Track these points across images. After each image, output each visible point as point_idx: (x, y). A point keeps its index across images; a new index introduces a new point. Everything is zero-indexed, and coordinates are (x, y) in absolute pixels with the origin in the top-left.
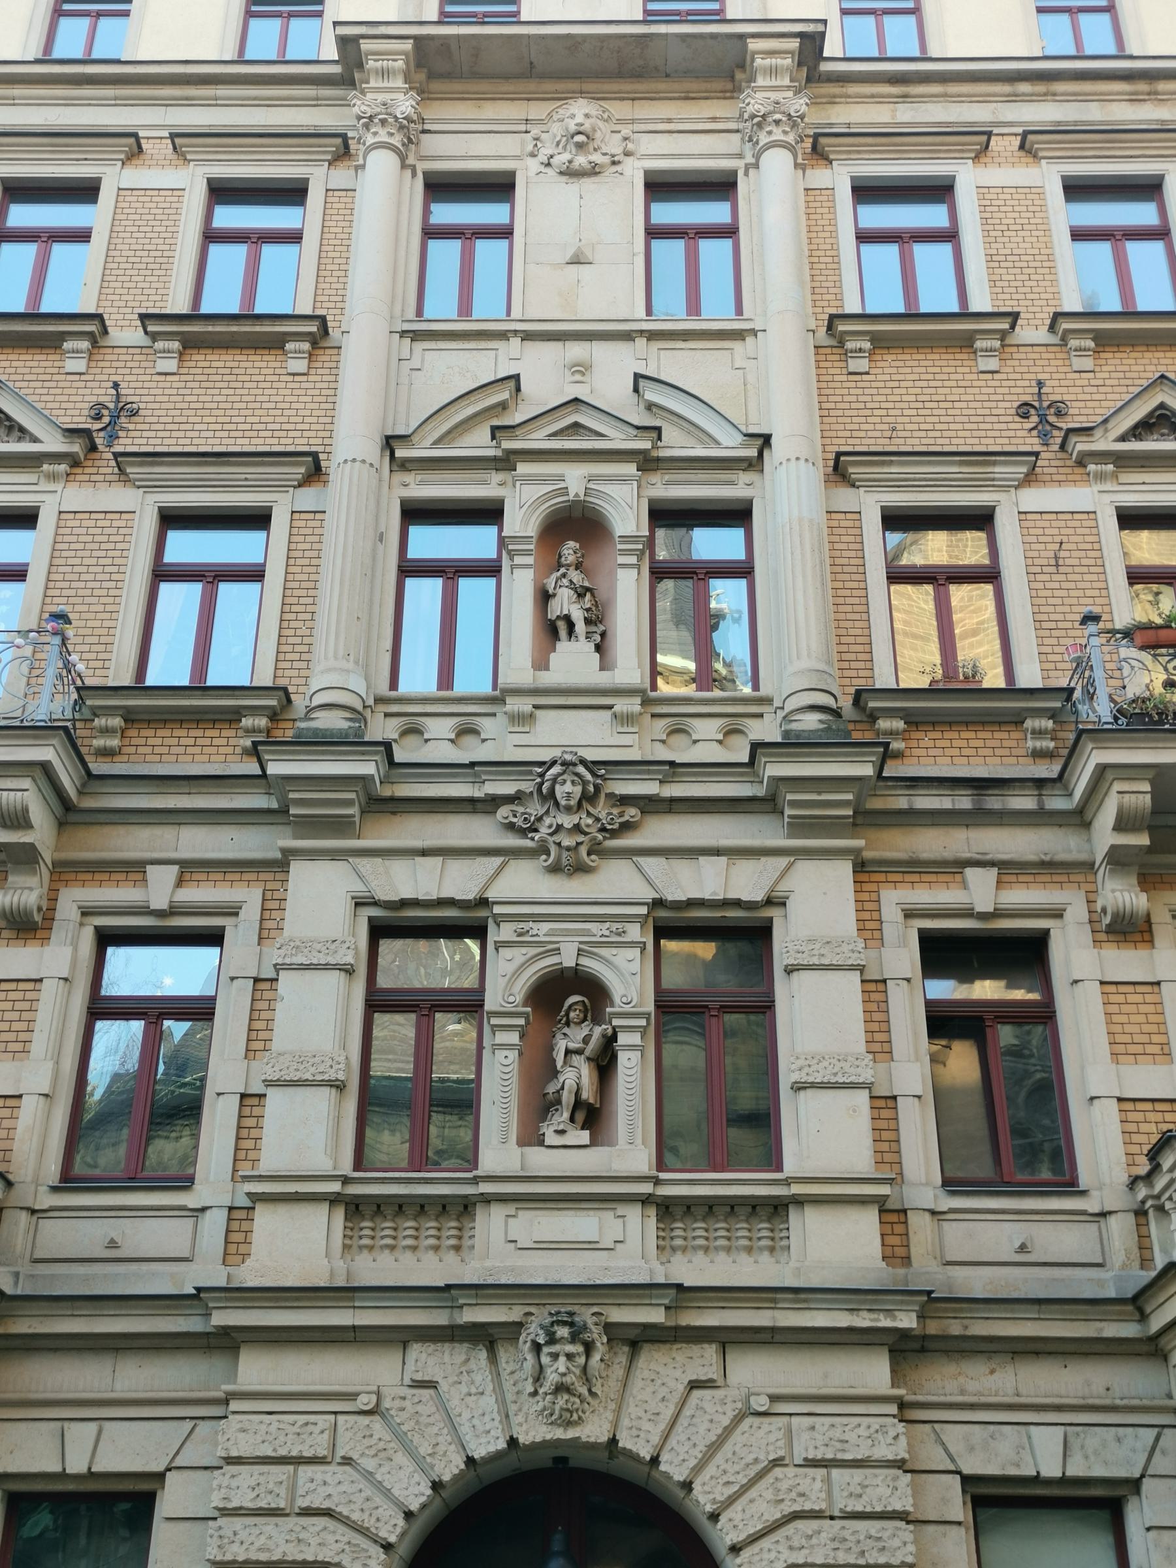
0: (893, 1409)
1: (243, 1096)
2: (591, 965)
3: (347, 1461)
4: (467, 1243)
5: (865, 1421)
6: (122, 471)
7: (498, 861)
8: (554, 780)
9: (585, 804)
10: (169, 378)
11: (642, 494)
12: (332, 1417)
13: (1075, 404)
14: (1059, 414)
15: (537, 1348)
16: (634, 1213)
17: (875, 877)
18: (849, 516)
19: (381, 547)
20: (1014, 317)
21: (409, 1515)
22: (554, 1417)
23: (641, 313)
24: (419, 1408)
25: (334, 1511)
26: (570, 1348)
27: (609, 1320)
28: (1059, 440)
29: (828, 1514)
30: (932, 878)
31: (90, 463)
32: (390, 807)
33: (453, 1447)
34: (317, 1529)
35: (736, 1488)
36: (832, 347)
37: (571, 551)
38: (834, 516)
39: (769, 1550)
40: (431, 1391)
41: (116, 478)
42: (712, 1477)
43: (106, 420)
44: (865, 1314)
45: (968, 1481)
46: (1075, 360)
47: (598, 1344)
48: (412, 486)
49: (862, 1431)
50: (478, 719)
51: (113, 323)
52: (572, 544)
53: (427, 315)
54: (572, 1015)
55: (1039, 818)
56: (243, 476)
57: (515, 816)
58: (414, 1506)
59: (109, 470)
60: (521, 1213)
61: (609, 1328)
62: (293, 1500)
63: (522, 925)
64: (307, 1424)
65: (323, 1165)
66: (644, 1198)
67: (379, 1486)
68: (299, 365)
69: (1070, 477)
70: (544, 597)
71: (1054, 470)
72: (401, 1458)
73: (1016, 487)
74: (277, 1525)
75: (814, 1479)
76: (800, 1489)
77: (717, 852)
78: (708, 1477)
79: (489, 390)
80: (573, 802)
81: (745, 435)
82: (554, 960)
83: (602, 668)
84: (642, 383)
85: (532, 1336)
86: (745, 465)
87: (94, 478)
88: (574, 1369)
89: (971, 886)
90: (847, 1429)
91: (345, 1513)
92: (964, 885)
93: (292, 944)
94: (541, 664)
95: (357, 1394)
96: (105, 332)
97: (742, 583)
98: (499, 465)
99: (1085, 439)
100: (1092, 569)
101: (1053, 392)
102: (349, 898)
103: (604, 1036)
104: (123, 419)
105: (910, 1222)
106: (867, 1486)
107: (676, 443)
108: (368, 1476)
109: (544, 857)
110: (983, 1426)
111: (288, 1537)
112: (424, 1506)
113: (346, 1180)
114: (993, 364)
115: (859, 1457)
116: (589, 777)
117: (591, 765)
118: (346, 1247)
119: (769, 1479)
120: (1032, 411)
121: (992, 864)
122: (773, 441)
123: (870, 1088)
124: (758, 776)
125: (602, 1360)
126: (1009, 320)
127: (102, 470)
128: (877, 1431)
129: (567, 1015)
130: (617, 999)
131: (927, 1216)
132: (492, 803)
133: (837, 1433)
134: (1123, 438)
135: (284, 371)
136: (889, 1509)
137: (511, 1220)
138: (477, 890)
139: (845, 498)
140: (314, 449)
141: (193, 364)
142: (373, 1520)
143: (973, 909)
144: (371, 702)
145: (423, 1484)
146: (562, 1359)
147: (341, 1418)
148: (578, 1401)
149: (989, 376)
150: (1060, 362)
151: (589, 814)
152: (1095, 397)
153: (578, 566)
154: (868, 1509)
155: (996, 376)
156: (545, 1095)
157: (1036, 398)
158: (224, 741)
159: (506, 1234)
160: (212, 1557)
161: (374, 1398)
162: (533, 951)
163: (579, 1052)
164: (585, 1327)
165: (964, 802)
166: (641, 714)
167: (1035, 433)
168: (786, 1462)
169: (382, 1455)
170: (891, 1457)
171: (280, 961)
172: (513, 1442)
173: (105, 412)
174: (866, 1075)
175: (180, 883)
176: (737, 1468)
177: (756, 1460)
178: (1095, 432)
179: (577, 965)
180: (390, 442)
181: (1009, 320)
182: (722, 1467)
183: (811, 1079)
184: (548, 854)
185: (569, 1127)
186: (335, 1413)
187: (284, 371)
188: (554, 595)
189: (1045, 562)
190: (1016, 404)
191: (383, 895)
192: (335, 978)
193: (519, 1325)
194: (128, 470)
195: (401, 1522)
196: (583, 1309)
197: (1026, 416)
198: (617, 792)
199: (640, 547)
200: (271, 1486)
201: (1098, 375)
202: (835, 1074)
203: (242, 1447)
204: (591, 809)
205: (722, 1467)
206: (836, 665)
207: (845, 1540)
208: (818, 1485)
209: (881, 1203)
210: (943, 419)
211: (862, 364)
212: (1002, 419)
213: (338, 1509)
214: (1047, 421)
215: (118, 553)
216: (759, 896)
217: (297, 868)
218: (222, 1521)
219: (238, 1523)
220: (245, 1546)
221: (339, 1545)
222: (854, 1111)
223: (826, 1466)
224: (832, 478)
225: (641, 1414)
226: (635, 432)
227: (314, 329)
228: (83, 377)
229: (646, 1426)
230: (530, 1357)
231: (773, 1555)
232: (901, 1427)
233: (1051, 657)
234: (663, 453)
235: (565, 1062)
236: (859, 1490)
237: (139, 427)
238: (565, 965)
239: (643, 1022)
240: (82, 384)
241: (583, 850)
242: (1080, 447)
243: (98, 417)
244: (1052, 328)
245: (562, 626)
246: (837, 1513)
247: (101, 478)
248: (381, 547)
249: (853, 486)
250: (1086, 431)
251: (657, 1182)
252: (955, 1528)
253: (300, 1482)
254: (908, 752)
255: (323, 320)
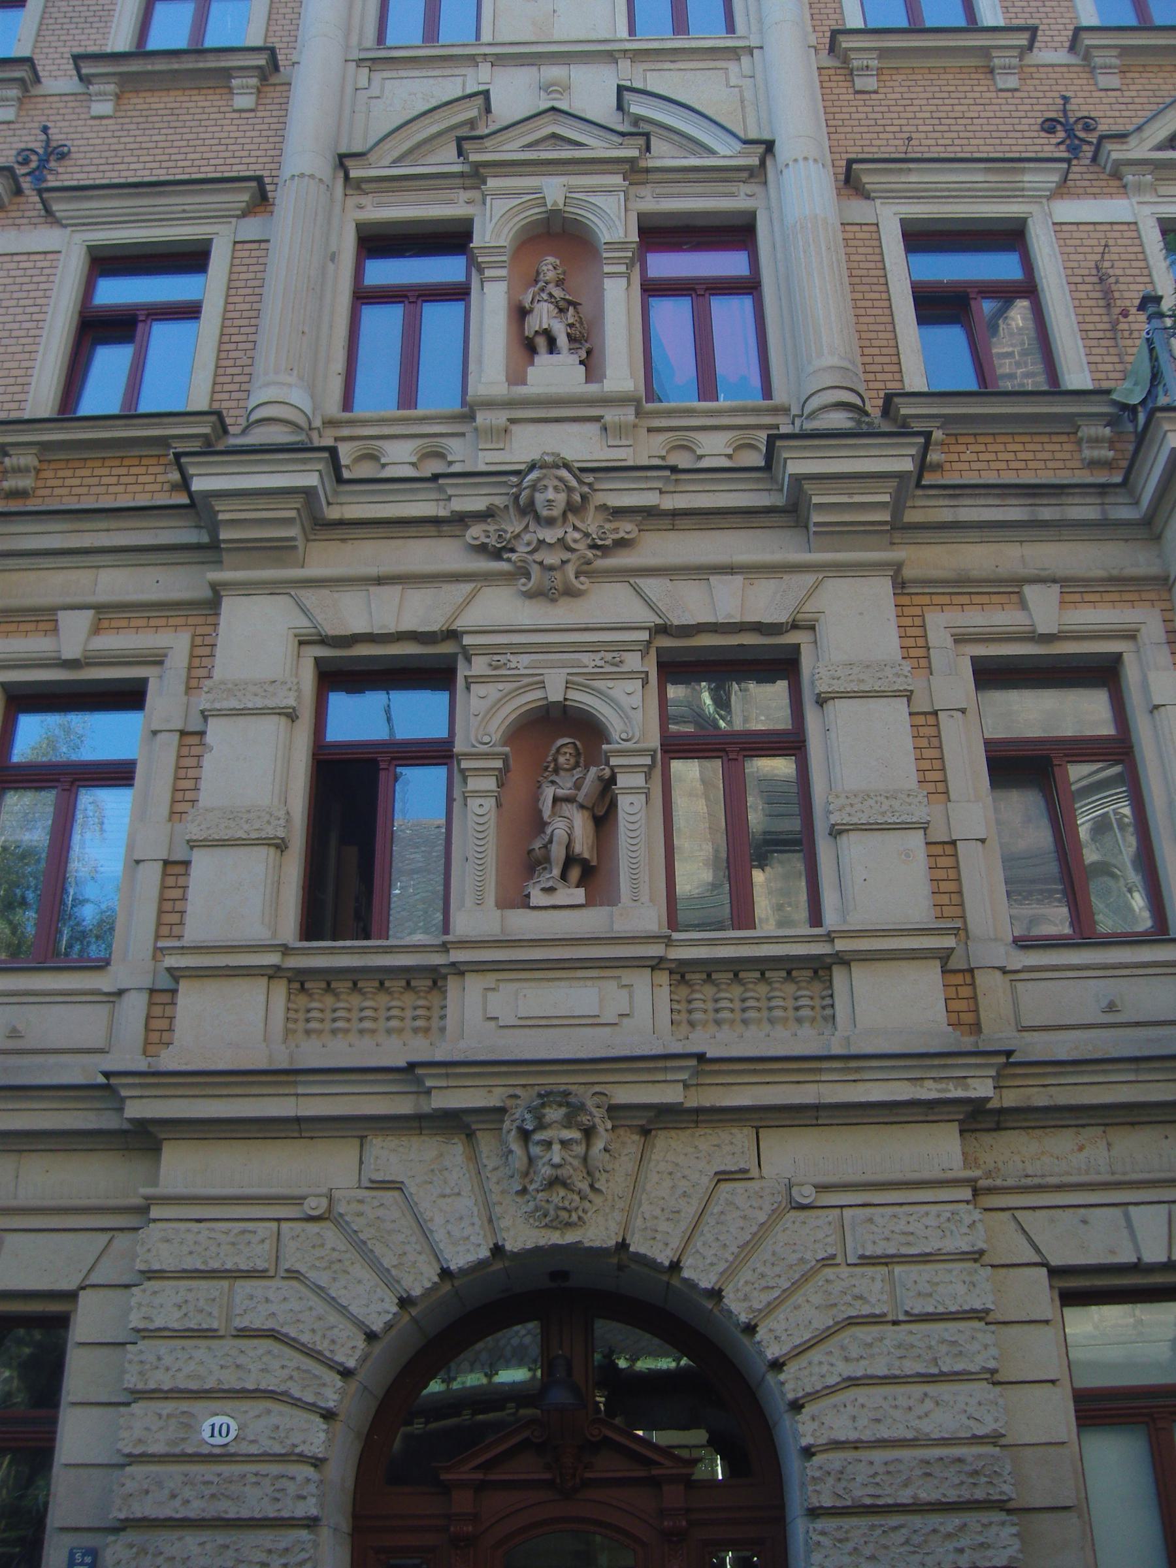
0: (967, 1194)
1: (166, 863)
2: (579, 698)
3: (294, 1275)
4: (435, 1023)
5: (934, 1209)
6: (48, 212)
7: (467, 587)
8: (534, 487)
9: (570, 516)
10: (104, 122)
11: (630, 206)
12: (274, 1225)
13: (1102, 120)
14: (1087, 128)
15: (525, 1136)
16: (641, 980)
17: (917, 600)
18: (865, 228)
19: (331, 267)
20: (1033, 31)
21: (371, 1337)
22: (548, 1219)
23: (623, 32)
24: (381, 1212)
25: (278, 1332)
26: (567, 1134)
27: (613, 1102)
28: (1090, 155)
29: (890, 1318)
30: (985, 599)
31: (15, 207)
32: (339, 533)
33: (423, 1258)
34: (260, 1351)
35: (776, 1293)
36: (836, 68)
37: (550, 267)
38: (848, 228)
39: (820, 1363)
40: (396, 1194)
41: (42, 220)
42: (746, 1282)
43: (34, 165)
44: (929, 1084)
45: (1055, 1272)
46: (1100, 78)
47: (601, 1129)
48: (370, 208)
49: (931, 1221)
50: (444, 440)
51: (46, 74)
52: (551, 259)
53: (389, 43)
54: (561, 760)
55: (1104, 528)
56: (180, 208)
57: (488, 537)
58: (377, 1326)
59: (35, 213)
60: (502, 985)
61: (614, 1110)
62: (229, 1319)
63: (497, 657)
64: (243, 1232)
65: (258, 932)
66: (654, 963)
67: (332, 1302)
68: (244, 101)
69: (1105, 190)
70: (521, 313)
71: (1087, 183)
72: (360, 1271)
73: (1049, 198)
74: (209, 1348)
75: (873, 1279)
76: (856, 1291)
77: (730, 570)
78: (742, 1282)
79: (456, 107)
80: (556, 512)
81: (745, 142)
82: (539, 694)
83: (589, 379)
84: (627, 96)
85: (518, 1123)
86: (745, 175)
87: (18, 221)
88: (570, 1159)
89: (1030, 605)
90: (911, 1219)
91: (293, 1335)
92: (1023, 605)
93: (223, 687)
94: (517, 377)
95: (304, 1198)
96: (37, 80)
97: (747, 302)
98: (468, 182)
99: (1118, 147)
100: (1139, 279)
101: (1080, 107)
102: (291, 638)
103: (600, 778)
104: (52, 164)
105: (978, 982)
106: (938, 1284)
107: (664, 155)
108: (319, 1290)
109: (523, 580)
110: (1071, 1210)
111: (222, 1362)
112: (389, 1326)
113: (286, 950)
114: (1012, 82)
115: (928, 1250)
116: (574, 483)
117: (577, 472)
118: (288, 1032)
119: (819, 1280)
120: (1059, 127)
121: (1054, 581)
122: (778, 147)
123: (925, 829)
124: (777, 483)
125: (606, 1150)
126: (1027, 35)
127: (27, 214)
128: (949, 1220)
129: (555, 760)
130: (615, 736)
131: (998, 974)
132: (462, 520)
133: (901, 1226)
134: (1159, 148)
135: (229, 109)
136: (966, 1307)
137: (490, 994)
138: (443, 620)
139: (859, 210)
140: (258, 173)
141: (129, 107)
142: (326, 1343)
143: (1034, 632)
144: (317, 423)
145: (387, 1300)
146: (556, 1147)
147: (285, 1226)
148: (577, 1198)
149: (1009, 94)
150: (1085, 82)
151: (575, 528)
152: (1125, 114)
153: (559, 283)
154: (941, 1309)
155: (1017, 94)
156: (530, 852)
157: (1061, 114)
158: (150, 479)
159: (485, 1010)
160: (131, 1386)
161: (324, 1202)
162: (509, 686)
163: (569, 800)
164: (582, 1108)
165: (1014, 512)
166: (635, 426)
167: (1062, 148)
168: (838, 1260)
169: (336, 1266)
170: (966, 1248)
171: (208, 706)
172: (497, 1250)
173: (34, 157)
174: (920, 813)
175: (96, 630)
176: (777, 1270)
177: (802, 1260)
178: (1129, 139)
179: (566, 699)
180: (342, 161)
181: (1027, 35)
182: (759, 1271)
183: (855, 820)
184: (529, 578)
185: (559, 885)
186: (278, 1220)
187: (229, 109)
188: (531, 311)
189: (1086, 272)
190: (1040, 121)
191: (331, 630)
192: (273, 726)
193: (501, 1111)
194: (55, 208)
195: (361, 1343)
196: (582, 1089)
197: (1051, 131)
198: (609, 504)
199: (630, 254)
200: (201, 1303)
201: (1126, 94)
202: (883, 814)
203: (165, 1259)
204: (579, 524)
205: (759, 1271)
206: (862, 376)
207: (912, 1346)
208: (878, 1285)
209: (944, 957)
210: (962, 135)
211: (870, 83)
212: (1026, 134)
213: (284, 1330)
214: (1076, 137)
215: (41, 294)
216: (782, 617)
217: (228, 604)
218: (142, 1344)
219: (163, 1347)
220: (171, 1373)
221: (286, 1371)
222: (907, 856)
223: (886, 1264)
224: (843, 192)
225: (658, 1212)
226: (619, 140)
227: (262, 62)
228: (12, 126)
229: (663, 1226)
230: (516, 1147)
231: (825, 1368)
232: (977, 1215)
233: (1101, 367)
234: (651, 164)
235: (553, 814)
236: (928, 1289)
237: (69, 169)
238: (551, 699)
239: (648, 761)
240: (11, 133)
241: (570, 570)
242: (1114, 155)
243: (26, 162)
244: (1072, 48)
245: (541, 342)
246: (902, 1317)
247: (25, 221)
248: (331, 267)
249: (868, 197)
250: (1122, 137)
251: (669, 942)
252: (1043, 1328)
253: (238, 1300)
254: (947, 466)
255: (272, 52)
